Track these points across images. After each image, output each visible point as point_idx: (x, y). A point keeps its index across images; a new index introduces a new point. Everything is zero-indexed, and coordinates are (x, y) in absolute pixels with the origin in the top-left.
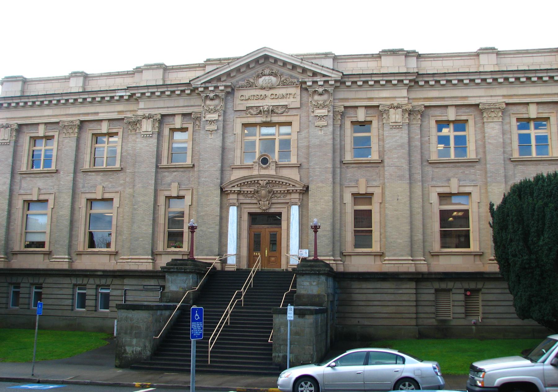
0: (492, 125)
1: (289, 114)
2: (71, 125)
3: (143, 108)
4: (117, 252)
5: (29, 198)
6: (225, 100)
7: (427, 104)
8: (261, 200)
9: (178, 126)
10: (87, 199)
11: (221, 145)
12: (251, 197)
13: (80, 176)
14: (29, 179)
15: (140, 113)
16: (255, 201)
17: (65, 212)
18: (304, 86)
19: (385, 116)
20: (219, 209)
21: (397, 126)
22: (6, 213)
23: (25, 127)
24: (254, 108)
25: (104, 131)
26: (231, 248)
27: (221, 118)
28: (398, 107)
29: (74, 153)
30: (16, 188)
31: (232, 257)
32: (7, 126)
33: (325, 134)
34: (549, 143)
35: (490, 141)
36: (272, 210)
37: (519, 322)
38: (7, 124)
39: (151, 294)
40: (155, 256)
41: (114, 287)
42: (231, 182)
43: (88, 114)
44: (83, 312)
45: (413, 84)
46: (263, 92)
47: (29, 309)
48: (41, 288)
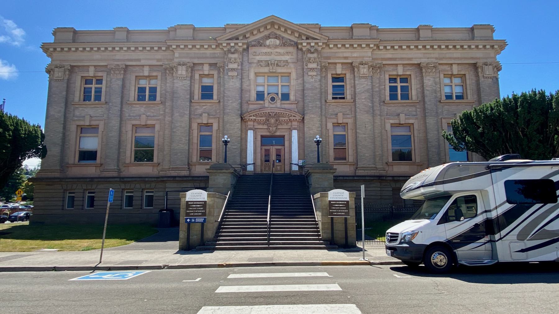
0: (428, 78)
6: (242, 54)
9: (206, 73)
11: (240, 86)
14: (81, 109)
17: (114, 134)
22: (61, 135)
25: (146, 74)
27: (240, 67)
28: (366, 64)
33: (315, 81)
35: (427, 88)
36: (278, 134)
45: (324, 46)
46: (269, 50)
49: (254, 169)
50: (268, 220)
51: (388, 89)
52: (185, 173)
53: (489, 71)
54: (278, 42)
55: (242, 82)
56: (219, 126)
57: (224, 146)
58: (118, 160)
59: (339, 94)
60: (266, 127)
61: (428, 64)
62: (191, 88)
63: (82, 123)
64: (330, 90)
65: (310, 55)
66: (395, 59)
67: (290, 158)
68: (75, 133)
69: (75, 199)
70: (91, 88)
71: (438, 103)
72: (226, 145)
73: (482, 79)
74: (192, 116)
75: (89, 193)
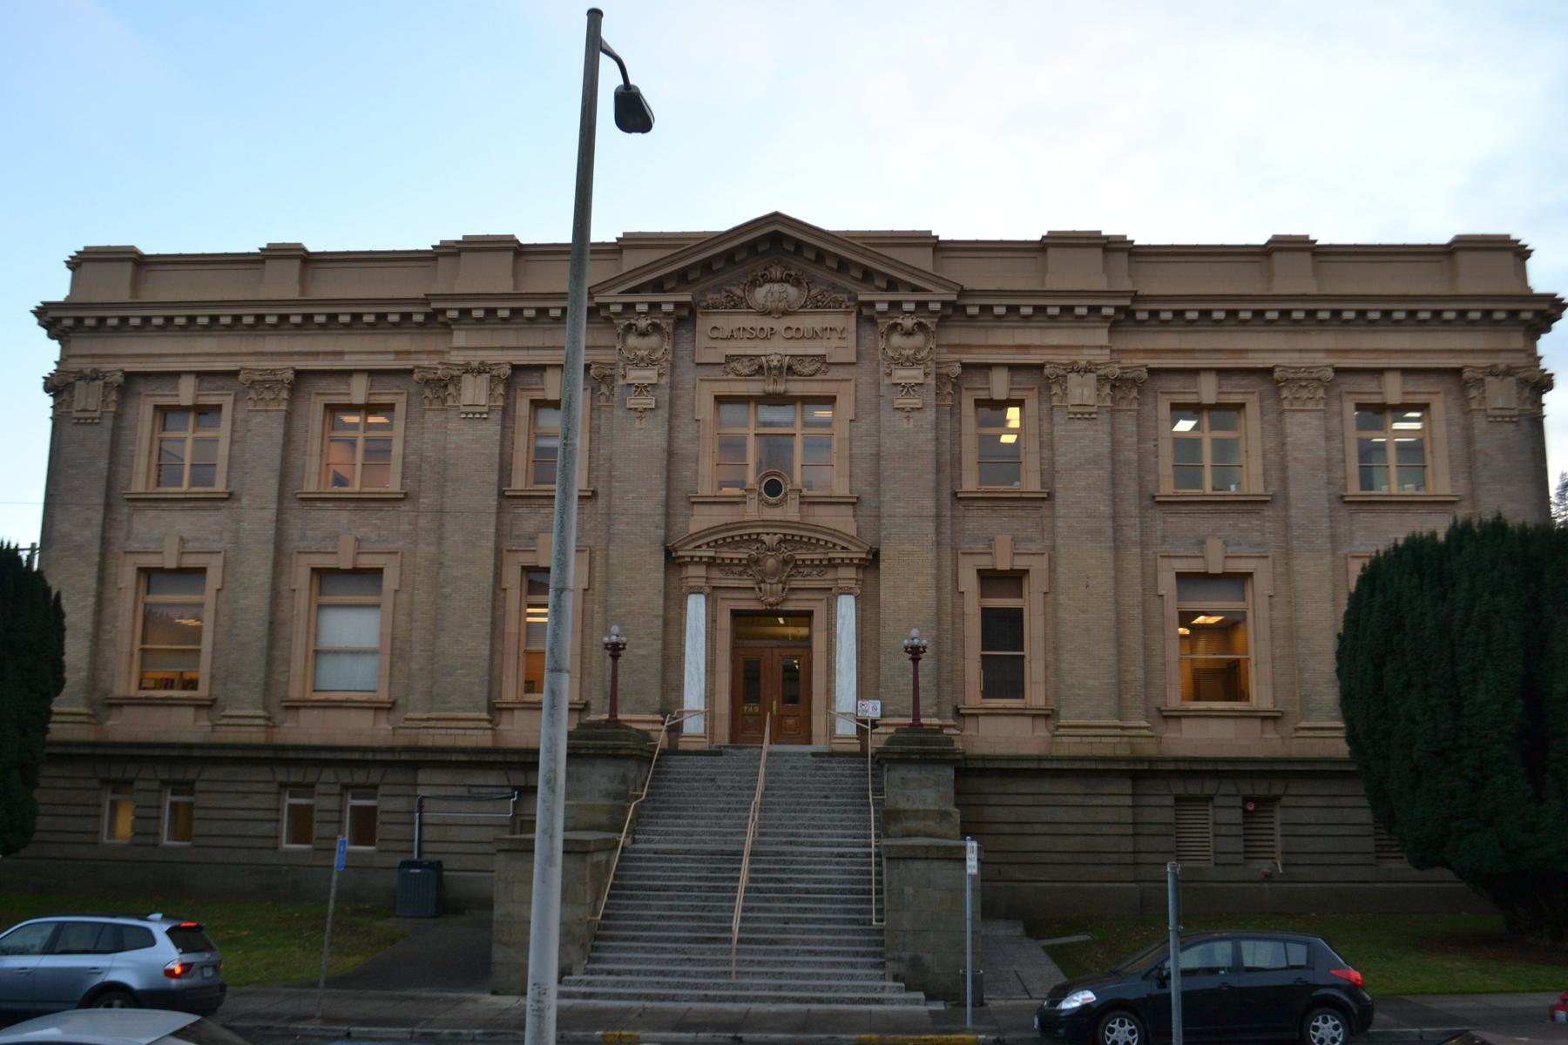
3: (464, 346)
7: (1154, 363)
8: (763, 581)
11: (665, 445)
12: (741, 574)
16: (749, 584)
20: (661, 601)
27: (664, 381)
28: (1087, 371)
39: (489, 806)
46: (767, 323)
50: (736, 925)
52: (483, 739)
55: (671, 429)
57: (609, 661)
62: (502, 446)
63: (152, 561)
72: (615, 657)
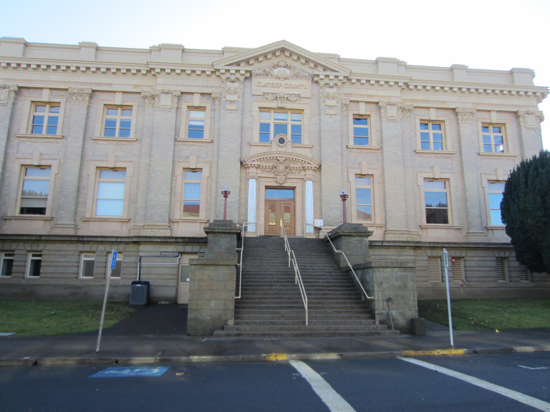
1: (301, 102)
2: (81, 93)
3: (162, 82)
4: (52, 218)
5: (28, 162)
7: (415, 105)
8: (278, 175)
10: (22, 165)
12: (269, 172)
13: (89, 143)
14: (28, 143)
15: (159, 88)
16: (272, 176)
17: (72, 178)
18: (316, 79)
19: (216, 102)
21: (393, 120)
23: (25, 90)
24: (270, 94)
26: (251, 218)
27: (240, 100)
28: (394, 105)
29: (84, 120)
30: (12, 151)
31: (252, 225)
32: (4, 87)
34: (369, 136)
37: (525, 283)
38: (4, 84)
40: (172, 224)
41: (126, 254)
42: (252, 157)
43: (100, 84)
44: (91, 280)
46: (278, 82)
47: (23, 278)
48: (12, 255)
49: (257, 230)
51: (481, 138)
53: (530, 120)
54: (288, 72)
56: (211, 172)
58: (76, 213)
59: (361, 137)
60: (272, 175)
61: (464, 109)
64: (352, 134)
65: (327, 90)
66: (427, 101)
67: (303, 217)
68: (17, 175)
69: (14, 263)
70: (43, 117)
71: (478, 156)
73: (524, 130)
74: (177, 159)
75: (33, 255)
